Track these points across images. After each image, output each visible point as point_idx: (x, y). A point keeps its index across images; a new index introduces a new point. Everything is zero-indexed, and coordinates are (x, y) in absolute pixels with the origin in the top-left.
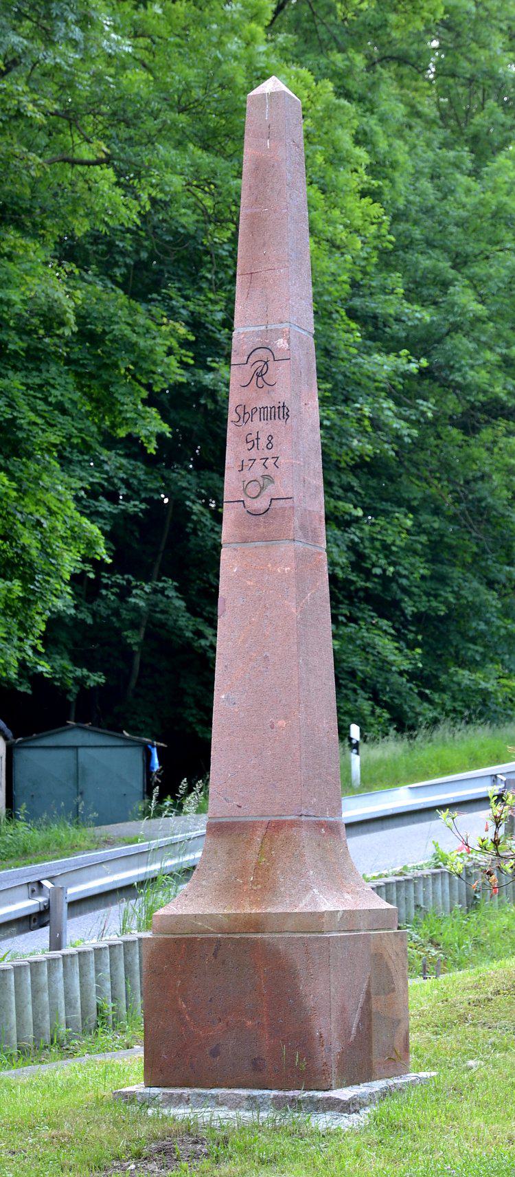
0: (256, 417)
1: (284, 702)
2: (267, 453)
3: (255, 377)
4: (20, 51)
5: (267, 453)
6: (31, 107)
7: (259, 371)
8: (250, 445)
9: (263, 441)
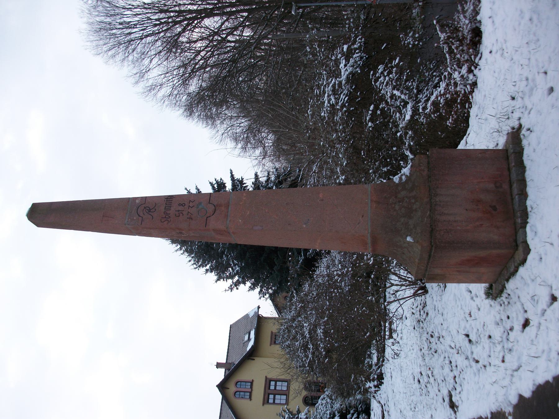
0: (168, 212)
3: (150, 213)
6: (438, 242)
7: (147, 211)
8: (181, 215)
9: (181, 208)
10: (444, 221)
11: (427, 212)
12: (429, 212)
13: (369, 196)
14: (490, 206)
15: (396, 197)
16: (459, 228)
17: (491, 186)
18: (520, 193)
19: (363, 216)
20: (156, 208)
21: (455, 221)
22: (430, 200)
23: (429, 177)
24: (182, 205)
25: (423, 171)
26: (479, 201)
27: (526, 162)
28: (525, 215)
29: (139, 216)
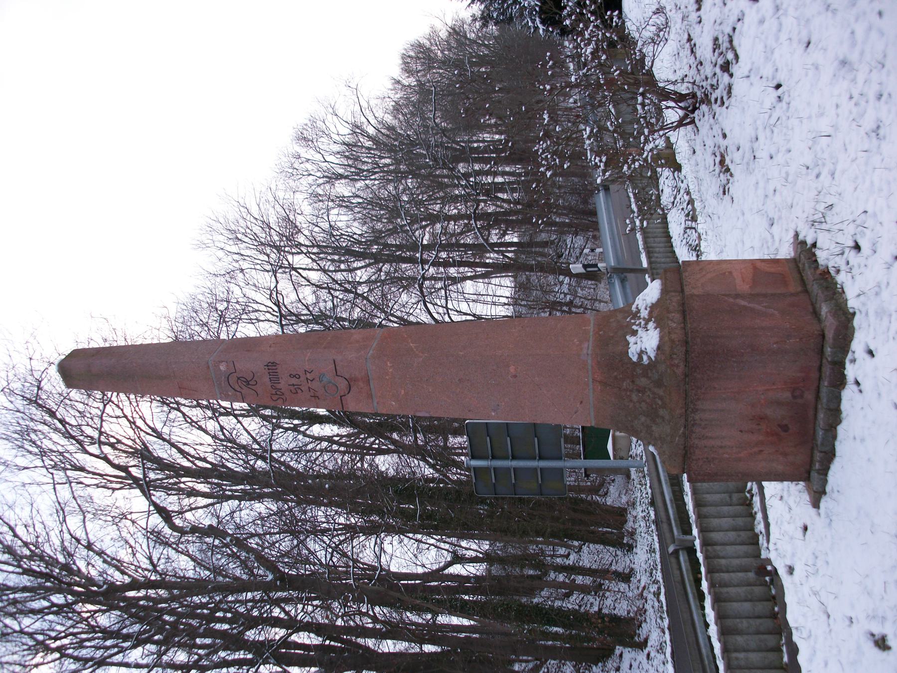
0: (278, 386)
1: (495, 367)
2: (303, 378)
4: (415, 83)
5: (303, 378)
8: (299, 391)
9: (294, 381)
10: (705, 447)
11: (680, 430)
12: (682, 429)
13: (590, 373)
14: (779, 425)
15: (633, 382)
16: (726, 456)
17: (787, 395)
18: (827, 428)
19: (581, 402)
20: (255, 378)
21: (721, 447)
22: (686, 411)
23: (686, 376)
24: (295, 376)
25: (678, 366)
26: (762, 418)
27: (840, 447)
28: (830, 455)
29: (236, 390)
